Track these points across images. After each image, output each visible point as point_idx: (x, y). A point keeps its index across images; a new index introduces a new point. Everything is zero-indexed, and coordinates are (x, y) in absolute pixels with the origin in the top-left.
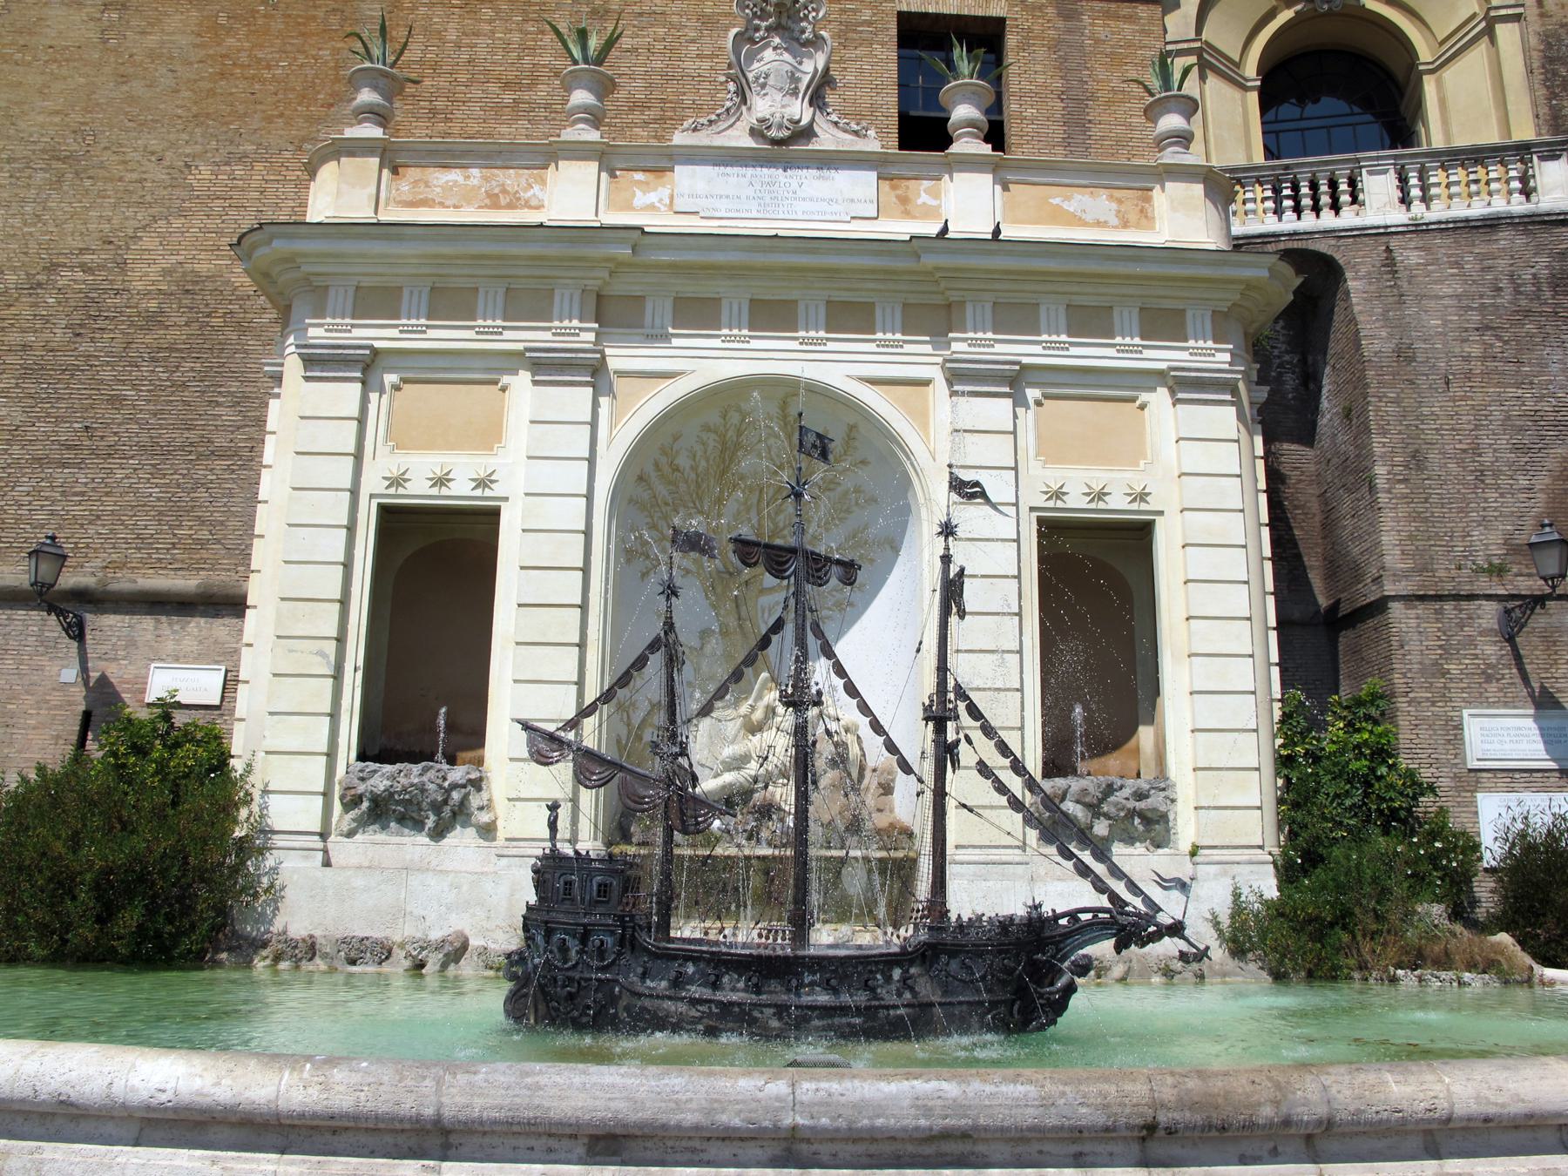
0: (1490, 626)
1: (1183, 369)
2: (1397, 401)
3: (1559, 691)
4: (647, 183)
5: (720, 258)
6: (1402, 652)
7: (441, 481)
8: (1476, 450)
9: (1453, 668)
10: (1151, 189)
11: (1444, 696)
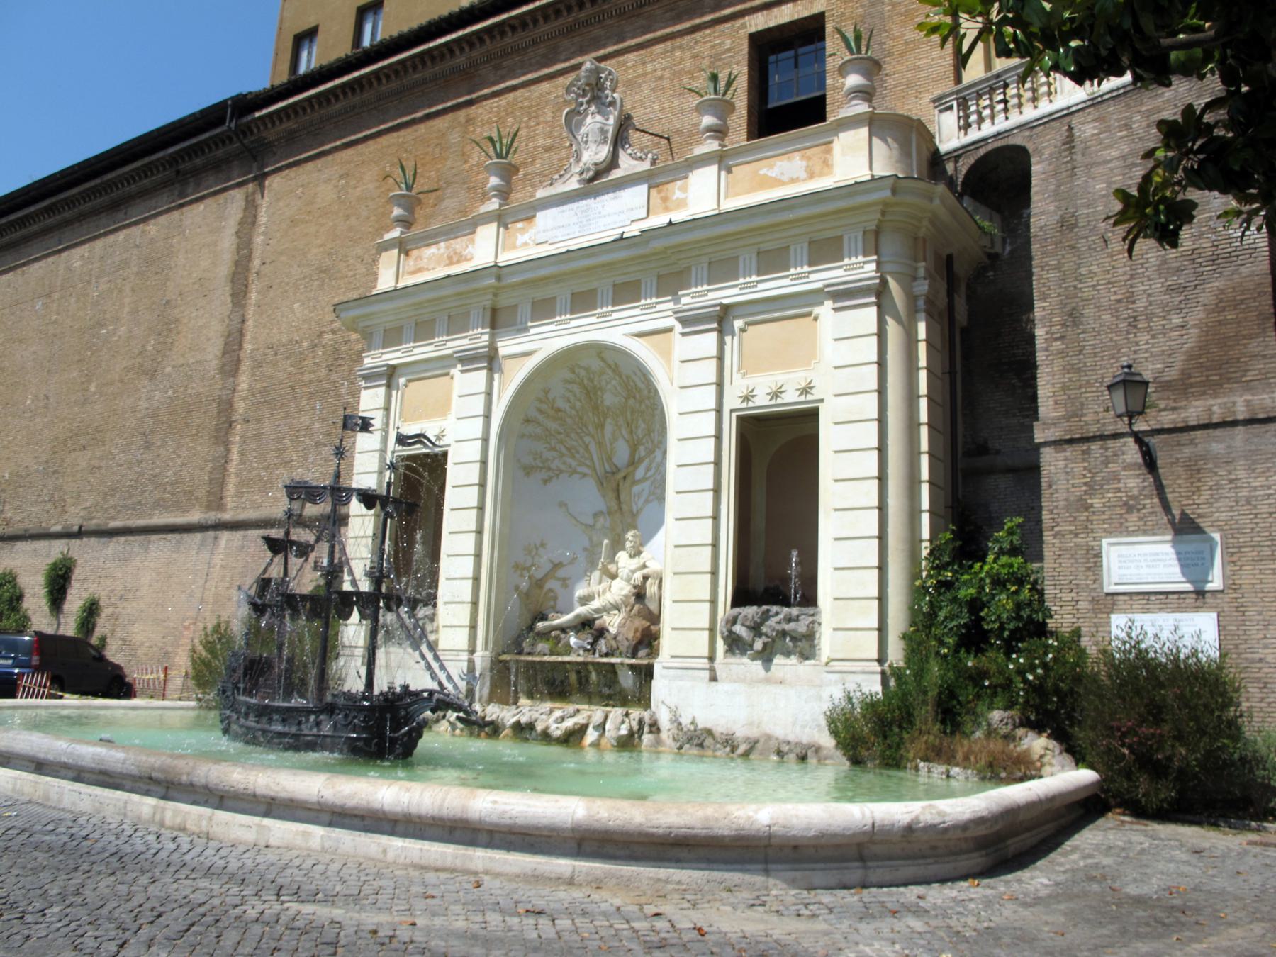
0: (1134, 461)
1: (833, 285)
2: (1057, 268)
3: (1200, 516)
4: (523, 229)
5: (543, 272)
6: (1051, 491)
7: (776, 395)
8: (1130, 298)
9: (1096, 502)
10: (831, 142)
11: (1087, 527)
